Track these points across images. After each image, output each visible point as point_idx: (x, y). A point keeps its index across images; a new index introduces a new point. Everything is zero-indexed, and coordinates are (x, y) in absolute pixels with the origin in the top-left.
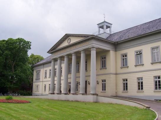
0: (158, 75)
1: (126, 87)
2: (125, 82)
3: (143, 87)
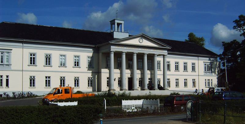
1: (32, 82)
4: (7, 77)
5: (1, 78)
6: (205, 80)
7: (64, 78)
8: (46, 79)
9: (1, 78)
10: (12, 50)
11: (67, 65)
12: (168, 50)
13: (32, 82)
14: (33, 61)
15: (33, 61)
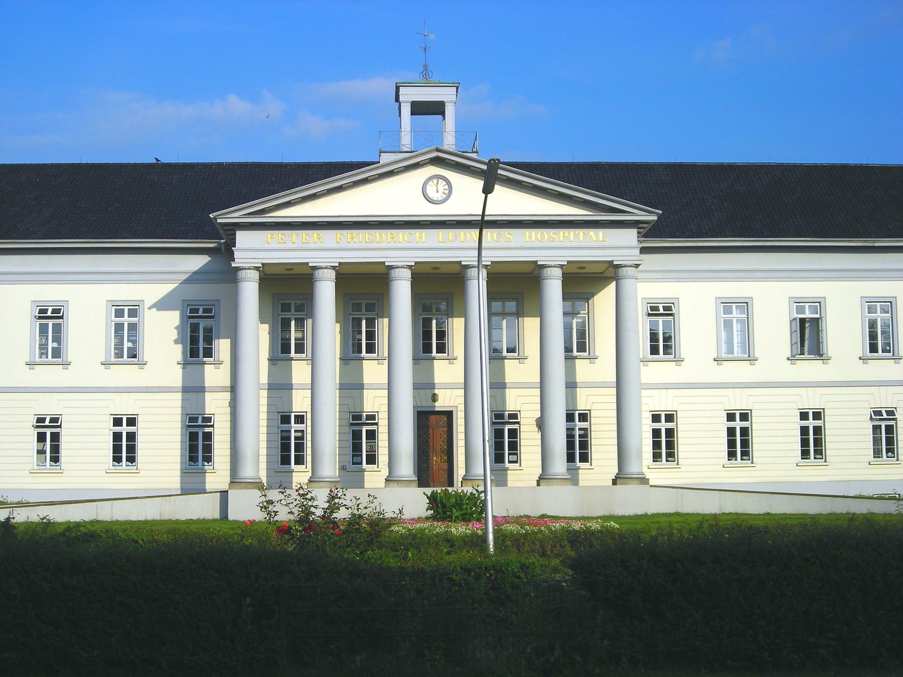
2: (811, 423)
3: (870, 438)
7: (890, 413)
8: (731, 424)
12: (649, 231)
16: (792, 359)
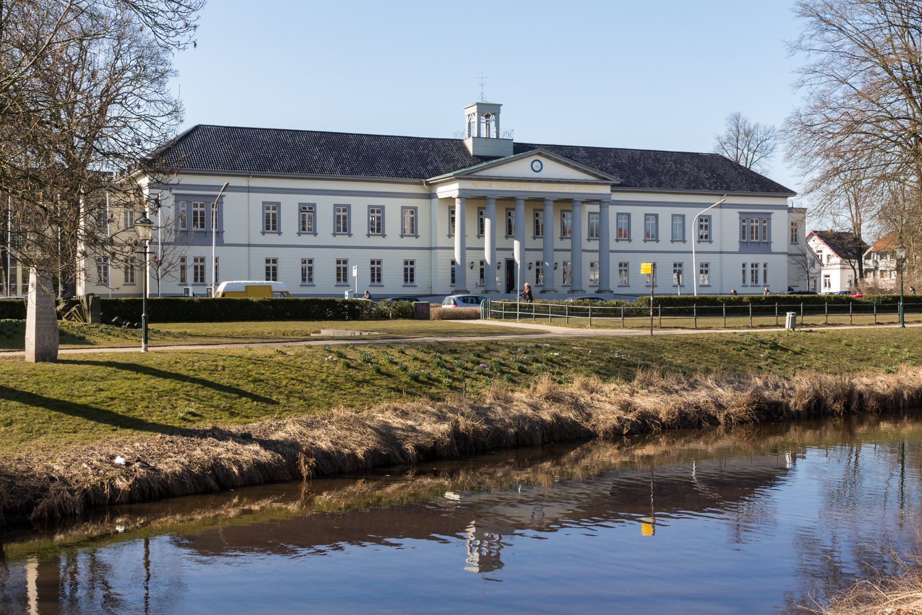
0: (310, 257)
1: (271, 272)
4: (765, 266)
5: (183, 264)
6: (744, 265)
9: (183, 264)
10: (770, 214)
11: (661, 236)
13: (271, 272)
14: (271, 223)
15: (271, 223)
16: (299, 234)
